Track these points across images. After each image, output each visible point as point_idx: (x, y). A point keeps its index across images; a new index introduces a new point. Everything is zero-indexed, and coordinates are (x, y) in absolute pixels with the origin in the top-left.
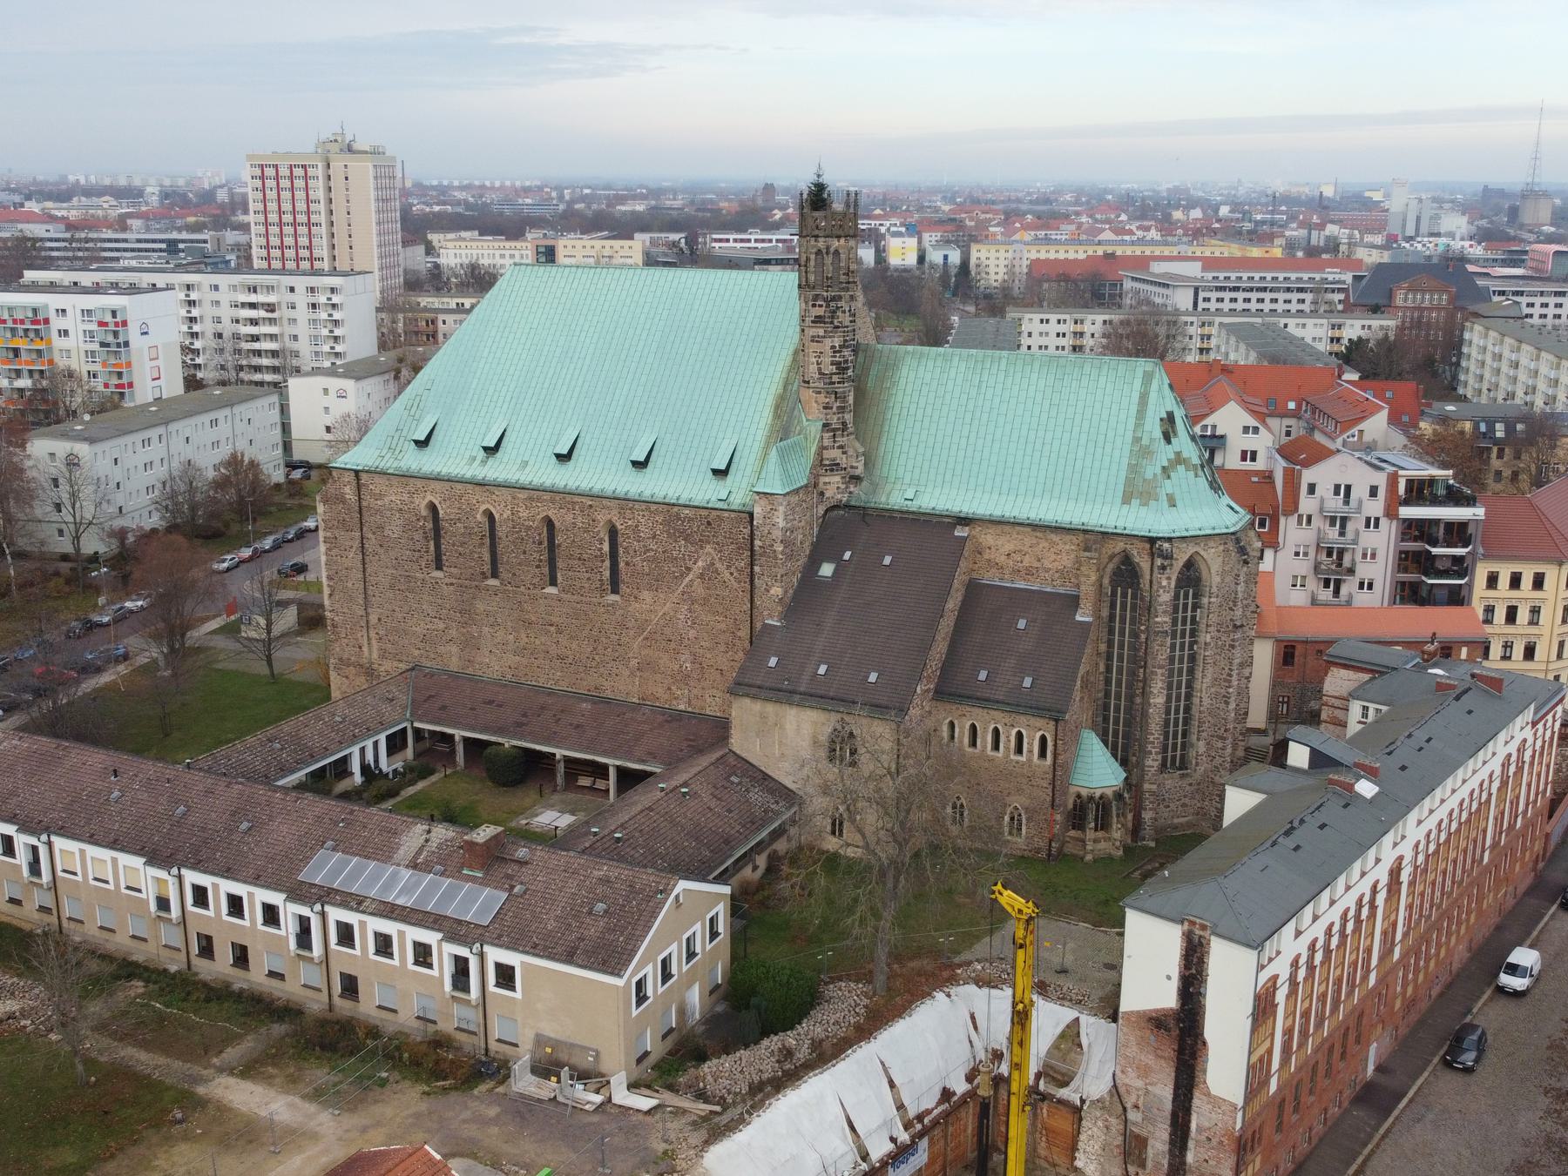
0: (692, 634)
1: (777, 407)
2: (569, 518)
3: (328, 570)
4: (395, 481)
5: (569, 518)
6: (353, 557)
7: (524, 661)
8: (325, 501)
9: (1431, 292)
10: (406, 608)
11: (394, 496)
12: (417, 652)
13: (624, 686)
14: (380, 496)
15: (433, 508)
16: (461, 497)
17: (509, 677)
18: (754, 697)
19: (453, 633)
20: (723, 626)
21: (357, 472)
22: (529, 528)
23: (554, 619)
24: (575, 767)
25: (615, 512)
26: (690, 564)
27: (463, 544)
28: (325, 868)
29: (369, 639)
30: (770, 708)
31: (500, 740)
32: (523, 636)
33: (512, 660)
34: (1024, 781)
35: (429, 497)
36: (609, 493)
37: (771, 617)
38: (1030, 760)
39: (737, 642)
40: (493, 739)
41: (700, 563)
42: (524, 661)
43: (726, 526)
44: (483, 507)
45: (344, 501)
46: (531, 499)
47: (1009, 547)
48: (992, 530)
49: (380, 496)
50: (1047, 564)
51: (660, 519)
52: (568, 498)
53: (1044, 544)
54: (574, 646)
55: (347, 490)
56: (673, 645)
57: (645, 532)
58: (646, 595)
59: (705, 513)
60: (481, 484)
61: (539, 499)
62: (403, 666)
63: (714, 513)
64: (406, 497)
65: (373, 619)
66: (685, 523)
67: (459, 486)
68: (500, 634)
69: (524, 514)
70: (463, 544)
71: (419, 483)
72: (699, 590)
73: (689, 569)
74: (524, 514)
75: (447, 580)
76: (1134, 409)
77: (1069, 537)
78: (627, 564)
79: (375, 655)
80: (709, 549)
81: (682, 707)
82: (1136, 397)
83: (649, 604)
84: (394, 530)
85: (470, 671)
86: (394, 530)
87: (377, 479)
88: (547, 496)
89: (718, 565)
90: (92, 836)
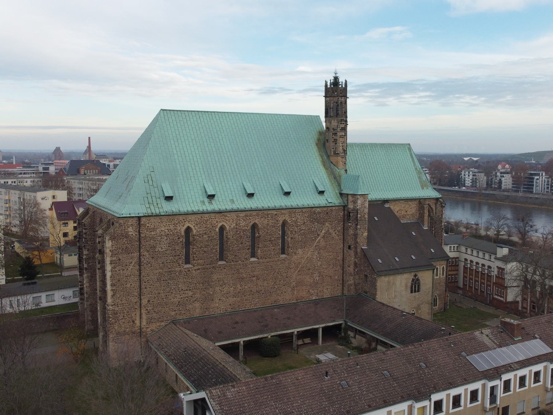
0: (319, 263)
1: (324, 166)
2: (266, 222)
3: (112, 280)
4: (165, 219)
5: (266, 222)
6: (133, 268)
7: (239, 299)
8: (112, 238)
9: (93, 169)
10: (168, 289)
11: (164, 228)
12: (173, 313)
13: (287, 297)
14: (154, 229)
15: (188, 230)
16: (207, 221)
17: (229, 310)
18: (386, 275)
19: (198, 295)
20: (332, 257)
21: (139, 218)
22: (244, 231)
23: (255, 273)
24: (302, 335)
25: (287, 215)
26: (319, 233)
27: (206, 246)
28: (482, 361)
29: (141, 314)
30: (391, 278)
31: (266, 335)
32: (239, 286)
33: (232, 300)
34: (438, 285)
35: (187, 224)
36: (285, 207)
37: (363, 245)
38: (440, 277)
39: (337, 262)
40: (261, 336)
41: (323, 232)
42: (239, 299)
43: (334, 213)
44: (220, 225)
45: (127, 236)
46: (246, 216)
47: (398, 209)
48: (393, 203)
49: (154, 229)
50: (408, 213)
51: (306, 215)
52: (265, 212)
53: (407, 206)
54: (265, 284)
55: (130, 229)
56: (311, 271)
57: (300, 222)
58: (300, 251)
59: (325, 209)
60: (220, 212)
61: (251, 215)
62: (163, 324)
63: (329, 208)
64: (172, 227)
65: (144, 302)
66: (313, 214)
67: (207, 215)
68: (226, 290)
69: (242, 223)
70: (206, 246)
71: (181, 218)
72: (323, 243)
73: (318, 235)
74: (242, 223)
75: (196, 268)
76: (411, 159)
77: (414, 202)
78: (292, 238)
79: (144, 323)
80: (327, 224)
81: (314, 298)
82: (409, 155)
83: (302, 255)
84: (162, 247)
85: (207, 314)
86: (162, 247)
87: (152, 219)
88: (254, 213)
89: (331, 231)
90: (385, 402)
